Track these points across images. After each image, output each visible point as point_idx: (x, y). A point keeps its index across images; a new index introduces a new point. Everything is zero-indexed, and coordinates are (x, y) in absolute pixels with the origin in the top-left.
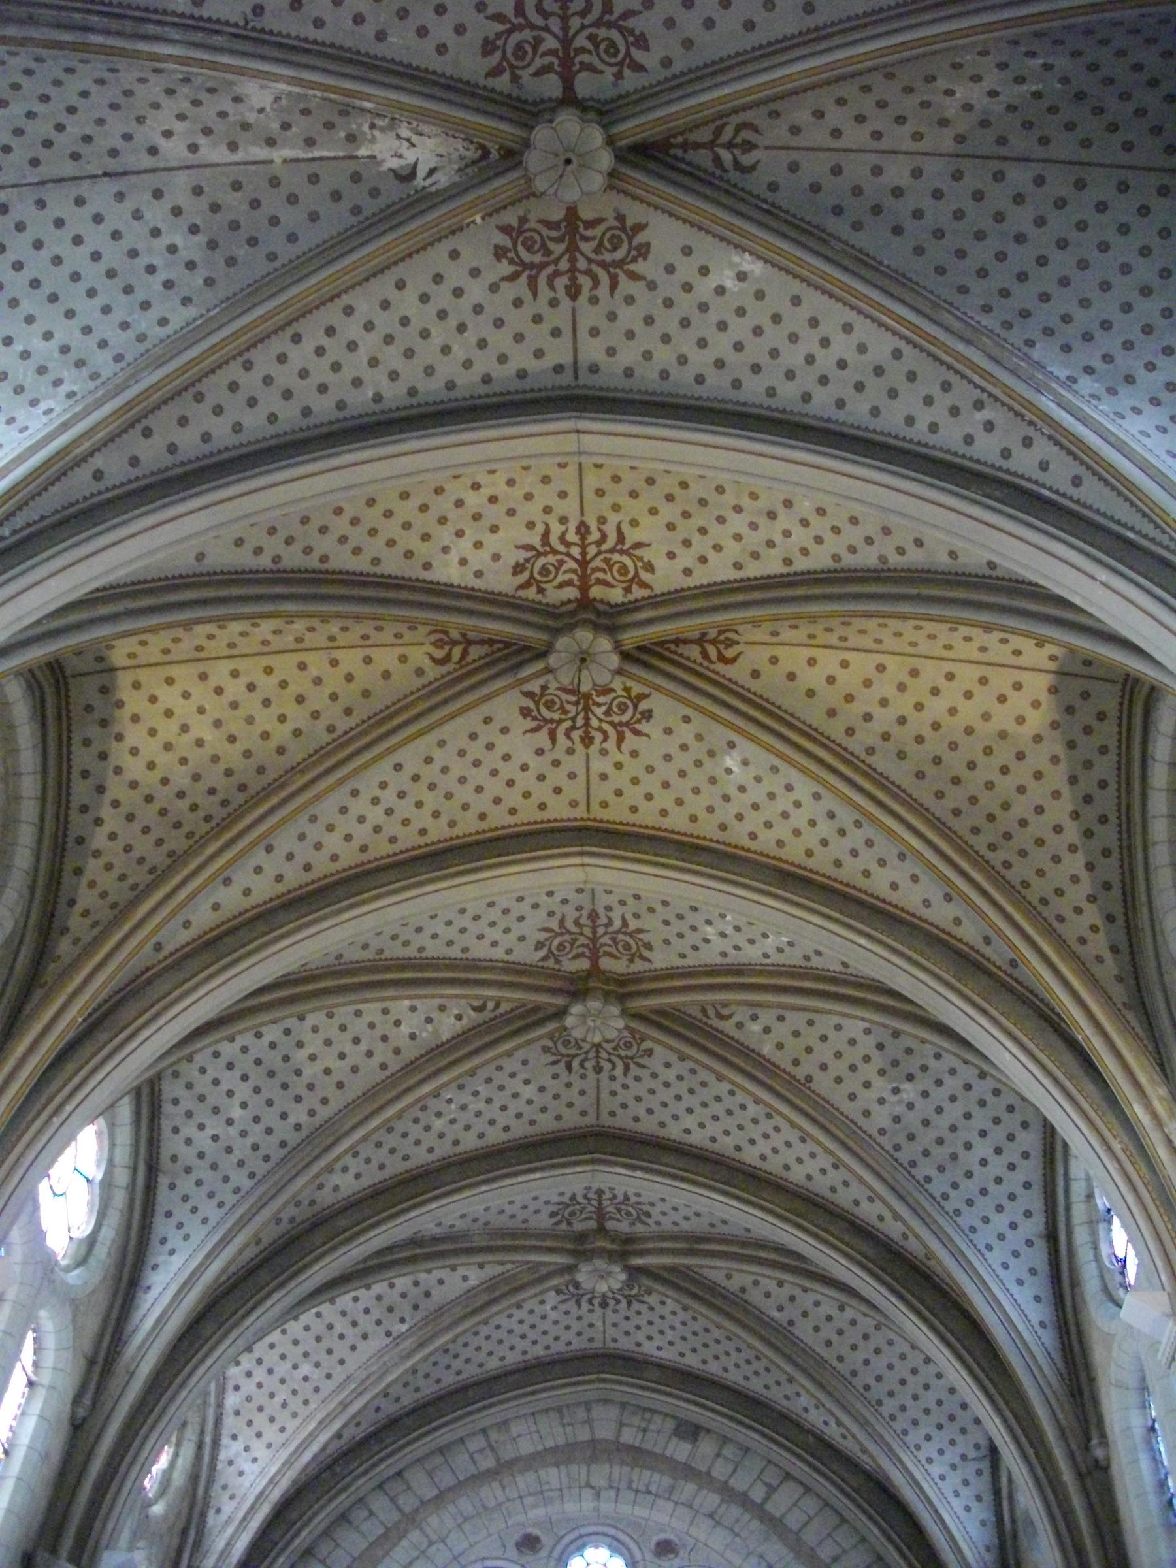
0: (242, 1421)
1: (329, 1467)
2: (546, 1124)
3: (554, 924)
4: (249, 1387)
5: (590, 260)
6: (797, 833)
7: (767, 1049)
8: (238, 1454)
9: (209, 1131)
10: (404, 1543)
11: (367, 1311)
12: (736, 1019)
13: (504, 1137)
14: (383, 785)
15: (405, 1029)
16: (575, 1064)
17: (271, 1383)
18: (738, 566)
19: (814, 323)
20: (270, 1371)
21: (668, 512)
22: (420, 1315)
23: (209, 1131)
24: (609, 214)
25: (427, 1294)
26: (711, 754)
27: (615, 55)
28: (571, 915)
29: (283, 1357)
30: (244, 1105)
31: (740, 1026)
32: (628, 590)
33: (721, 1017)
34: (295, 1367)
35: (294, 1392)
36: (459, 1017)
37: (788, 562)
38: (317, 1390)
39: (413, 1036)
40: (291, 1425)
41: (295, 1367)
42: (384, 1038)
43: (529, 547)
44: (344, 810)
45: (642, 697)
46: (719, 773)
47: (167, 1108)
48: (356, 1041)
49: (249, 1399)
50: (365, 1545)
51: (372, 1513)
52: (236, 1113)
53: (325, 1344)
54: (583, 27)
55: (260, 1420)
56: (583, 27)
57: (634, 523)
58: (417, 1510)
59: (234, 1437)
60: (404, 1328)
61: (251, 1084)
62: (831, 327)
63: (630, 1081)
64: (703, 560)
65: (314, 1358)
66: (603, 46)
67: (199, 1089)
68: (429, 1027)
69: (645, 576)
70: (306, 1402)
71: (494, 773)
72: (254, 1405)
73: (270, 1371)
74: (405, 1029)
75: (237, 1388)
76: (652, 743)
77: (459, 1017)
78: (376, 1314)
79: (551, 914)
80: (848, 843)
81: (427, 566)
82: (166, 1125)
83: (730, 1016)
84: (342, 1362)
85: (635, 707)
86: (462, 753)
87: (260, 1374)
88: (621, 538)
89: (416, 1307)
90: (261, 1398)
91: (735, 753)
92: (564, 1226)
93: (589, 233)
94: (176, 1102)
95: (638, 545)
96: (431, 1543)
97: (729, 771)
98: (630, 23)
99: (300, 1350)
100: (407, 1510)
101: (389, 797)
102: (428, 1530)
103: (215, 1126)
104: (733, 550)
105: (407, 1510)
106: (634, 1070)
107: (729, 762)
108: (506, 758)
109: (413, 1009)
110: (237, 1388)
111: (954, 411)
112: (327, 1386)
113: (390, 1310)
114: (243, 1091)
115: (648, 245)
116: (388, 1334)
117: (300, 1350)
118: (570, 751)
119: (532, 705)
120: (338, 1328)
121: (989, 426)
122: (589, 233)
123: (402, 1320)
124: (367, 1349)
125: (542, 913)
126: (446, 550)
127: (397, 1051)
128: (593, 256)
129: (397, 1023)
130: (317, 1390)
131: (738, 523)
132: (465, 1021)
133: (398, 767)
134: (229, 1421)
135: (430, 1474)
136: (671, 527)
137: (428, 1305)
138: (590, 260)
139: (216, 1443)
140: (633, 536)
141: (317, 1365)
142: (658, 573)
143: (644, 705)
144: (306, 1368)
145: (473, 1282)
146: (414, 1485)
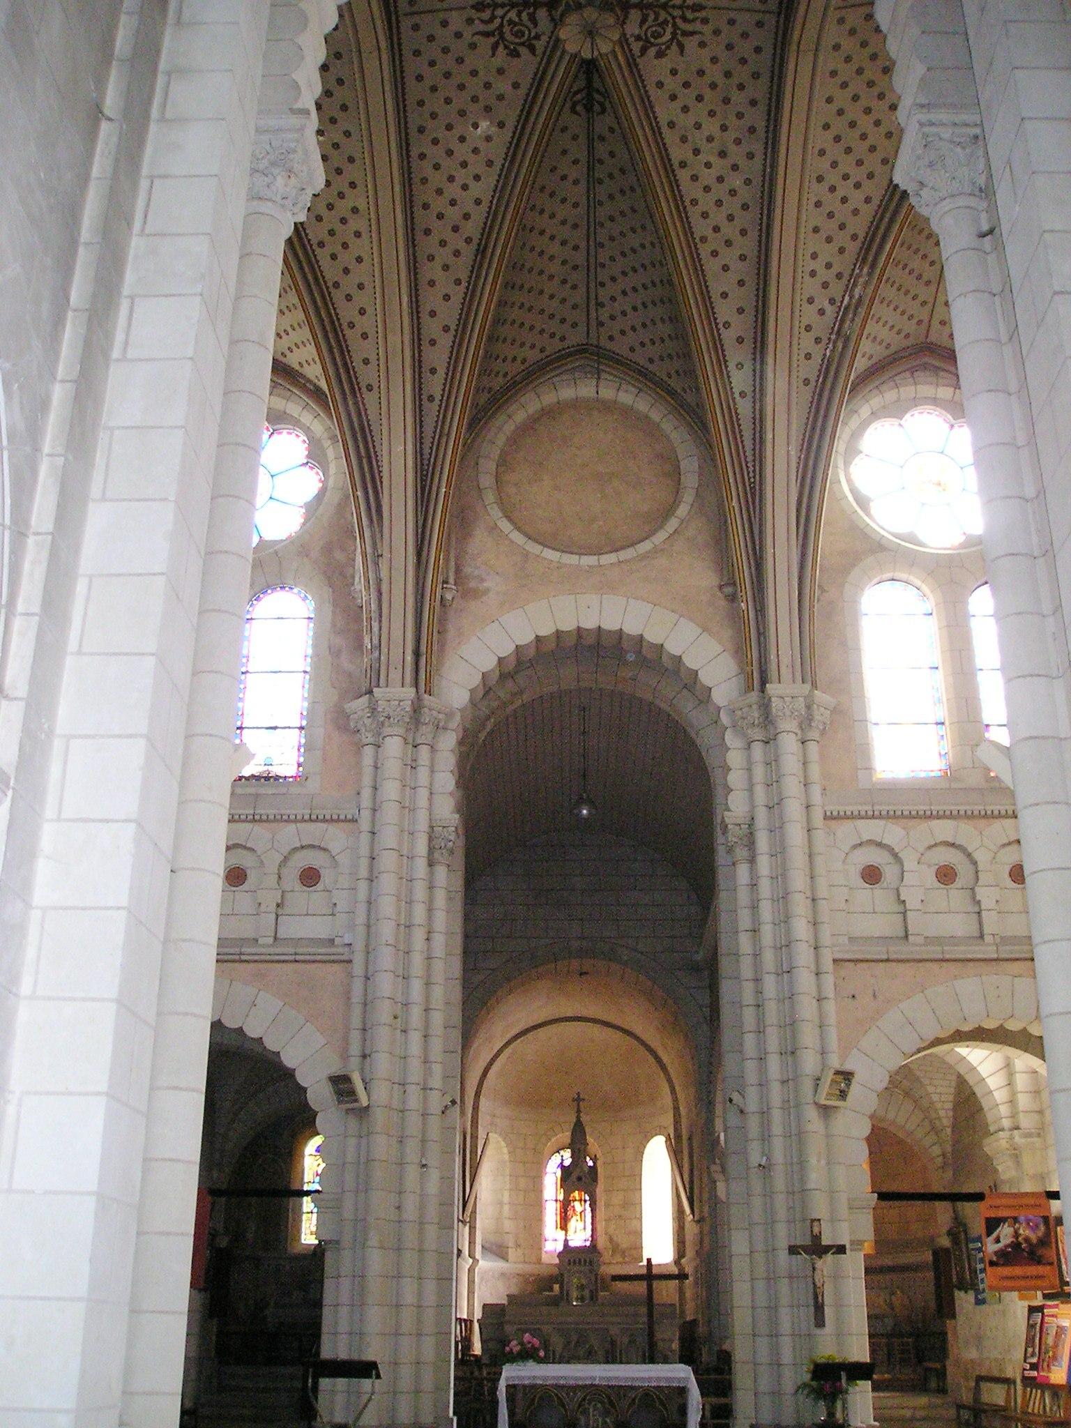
5: (502, 18)
6: (439, 192)
18: (671, 125)
19: (477, 178)
21: (715, 73)
24: (539, 29)
26: (488, 109)
27: (653, 36)
32: (638, 38)
37: (683, 165)
45: (532, 49)
46: (471, 118)
54: (674, 18)
56: (674, 18)
57: (702, 45)
62: (476, 190)
64: (673, 97)
66: (660, 29)
69: (652, 51)
76: (484, 60)
80: (449, 235)
85: (523, 44)
88: (685, 34)
91: (494, 129)
93: (524, 15)
95: (681, 47)
97: (476, 126)
98: (674, 47)
104: (686, 121)
107: (484, 125)
111: (825, 285)
115: (518, 55)
121: (822, 312)
122: (524, 15)
128: (507, 18)
131: (710, 126)
136: (701, 73)
138: (502, 18)
140: (691, 44)
142: (656, 62)
143: (523, 51)
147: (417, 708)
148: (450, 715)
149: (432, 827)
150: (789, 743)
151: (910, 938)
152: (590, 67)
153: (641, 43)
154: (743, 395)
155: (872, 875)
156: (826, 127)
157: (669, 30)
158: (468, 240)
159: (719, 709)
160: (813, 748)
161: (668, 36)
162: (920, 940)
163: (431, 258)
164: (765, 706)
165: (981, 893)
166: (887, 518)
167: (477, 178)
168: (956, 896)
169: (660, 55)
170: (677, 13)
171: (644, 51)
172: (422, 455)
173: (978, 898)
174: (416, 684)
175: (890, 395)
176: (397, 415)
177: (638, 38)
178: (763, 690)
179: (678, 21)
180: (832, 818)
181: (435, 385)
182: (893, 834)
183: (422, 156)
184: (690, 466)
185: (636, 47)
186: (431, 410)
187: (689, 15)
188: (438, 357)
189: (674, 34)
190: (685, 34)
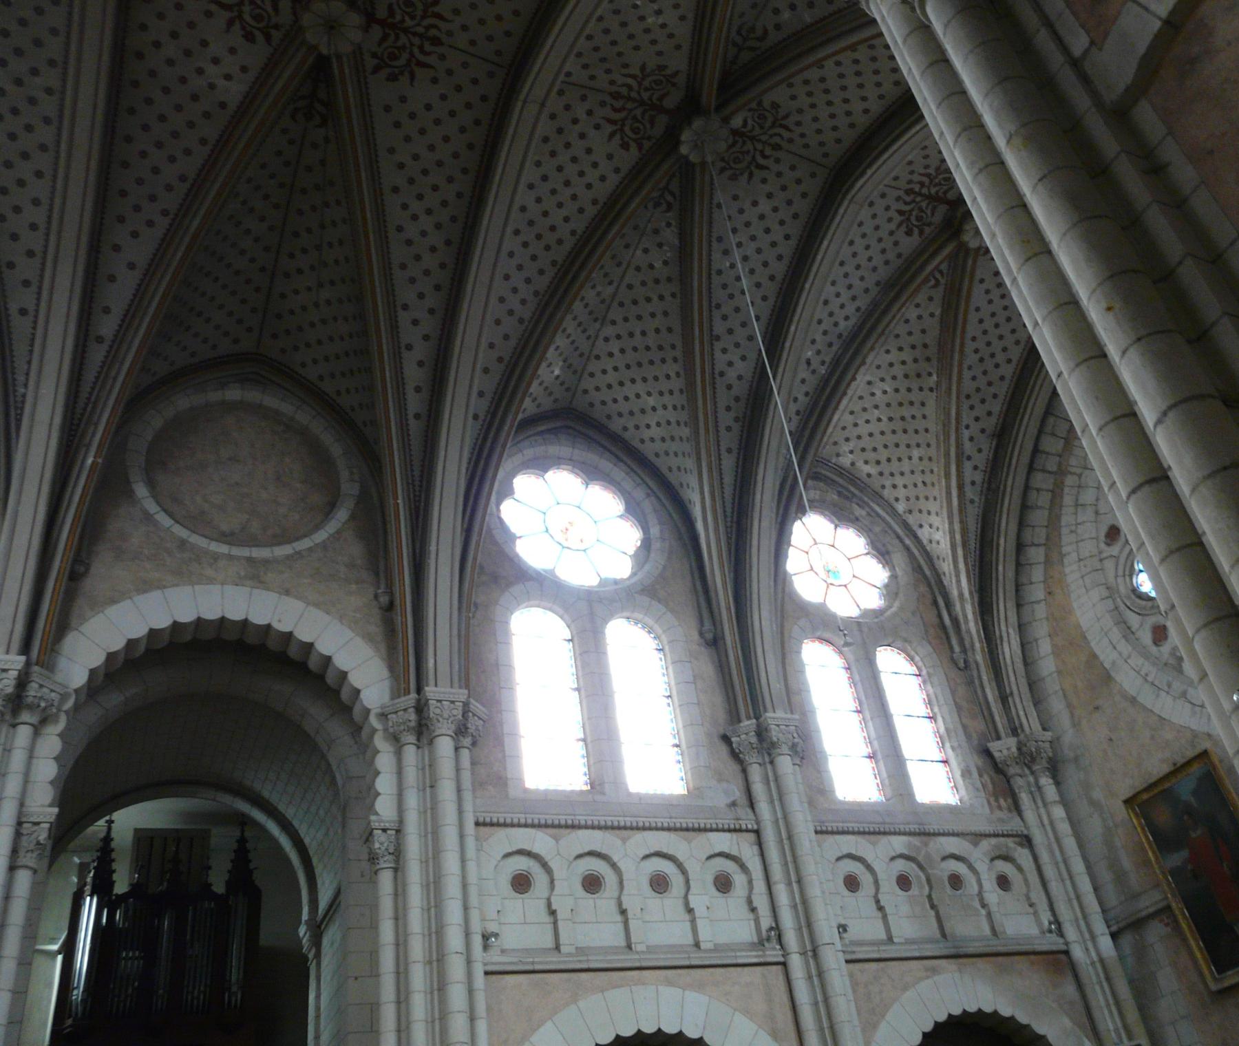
0: (916, 513)
1: (989, 489)
2: (803, 207)
3: (609, 128)
4: (901, 493)
7: (808, 18)
8: (930, 534)
9: (653, 424)
10: (1066, 490)
11: (909, 390)
12: (770, 28)
13: (793, 242)
14: (405, 207)
15: (658, 264)
16: (761, 161)
17: (908, 479)
20: (902, 474)
22: (934, 362)
23: (653, 424)
25: (925, 346)
28: (607, 112)
29: (900, 460)
30: (649, 394)
31: (778, 27)
33: (761, 39)
34: (910, 458)
35: (923, 472)
36: (669, 225)
38: (930, 459)
39: (665, 263)
40: (936, 492)
41: (910, 458)
42: (657, 281)
43: (230, 23)
44: (409, 242)
47: (627, 436)
48: (648, 300)
49: (908, 499)
50: (1046, 513)
51: (1038, 490)
52: (651, 401)
53: (911, 431)
55: (922, 504)
58: (1060, 464)
59: (921, 526)
60: (935, 377)
61: (639, 381)
63: (799, 130)
65: (913, 443)
67: (625, 411)
68: (665, 248)
70: (932, 471)
71: (437, 122)
72: (913, 500)
73: (902, 474)
74: (658, 264)
75: (897, 500)
77: (669, 225)
78: (915, 386)
79: (597, 127)
81: (223, 105)
82: (636, 443)
83: (766, 31)
84: (927, 431)
86: (408, 139)
87: (899, 481)
88: (419, 64)
89: (928, 359)
90: (912, 492)
92: (927, 230)
94: (625, 429)
96: (1080, 476)
99: (903, 447)
100: (1055, 469)
101: (416, 206)
102: (1073, 470)
103: (652, 419)
105: (1055, 469)
106: (789, 122)
108: (428, 107)
109: (646, 251)
110: (897, 500)
112: (932, 452)
113: (919, 376)
114: (640, 387)
116: (931, 390)
117: (903, 447)
118: (442, 57)
119: (388, 71)
120: (907, 415)
123: (930, 374)
124: (930, 409)
125: (592, 133)
126: (212, 86)
127: (669, 280)
129: (651, 267)
130: (930, 459)
132: (673, 223)
133: (396, 190)
134: (911, 520)
135: (1053, 434)
137: (932, 351)
139: (916, 537)
141: (918, 445)
143: (260, 37)
144: (916, 453)
145: (938, 312)
146: (1047, 450)
147: (22, 682)
148: (64, 697)
149: (20, 824)
150: (445, 746)
151: (562, 948)
152: (321, 68)
153: (376, 61)
154: (417, 416)
155: (521, 883)
156: (531, 187)
157: (405, 56)
158: (165, 213)
159: (368, 711)
160: (465, 754)
161: (402, 61)
162: (572, 950)
163: (123, 194)
164: (421, 708)
165: (694, 901)
166: (532, 550)
167: (188, 152)
168: (671, 902)
169: (393, 78)
170: (416, 41)
171: (376, 70)
172: (73, 413)
173: (554, 907)
174: (25, 649)
175: (540, 450)
176: (50, 368)
177: (374, 55)
178: (419, 690)
179: (416, 50)
180: (485, 824)
181: (107, 327)
182: (540, 842)
183: (132, 111)
184: (350, 489)
185: (370, 63)
186: (97, 355)
187: (427, 47)
188: (117, 296)
189: (409, 61)
190: (419, 64)
